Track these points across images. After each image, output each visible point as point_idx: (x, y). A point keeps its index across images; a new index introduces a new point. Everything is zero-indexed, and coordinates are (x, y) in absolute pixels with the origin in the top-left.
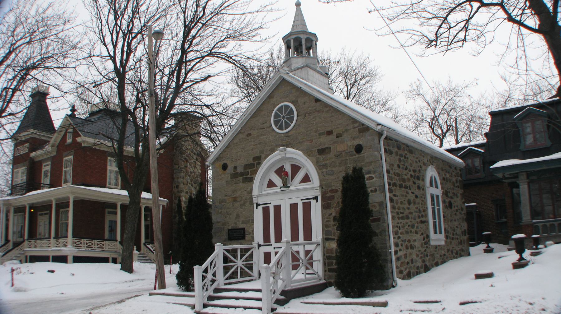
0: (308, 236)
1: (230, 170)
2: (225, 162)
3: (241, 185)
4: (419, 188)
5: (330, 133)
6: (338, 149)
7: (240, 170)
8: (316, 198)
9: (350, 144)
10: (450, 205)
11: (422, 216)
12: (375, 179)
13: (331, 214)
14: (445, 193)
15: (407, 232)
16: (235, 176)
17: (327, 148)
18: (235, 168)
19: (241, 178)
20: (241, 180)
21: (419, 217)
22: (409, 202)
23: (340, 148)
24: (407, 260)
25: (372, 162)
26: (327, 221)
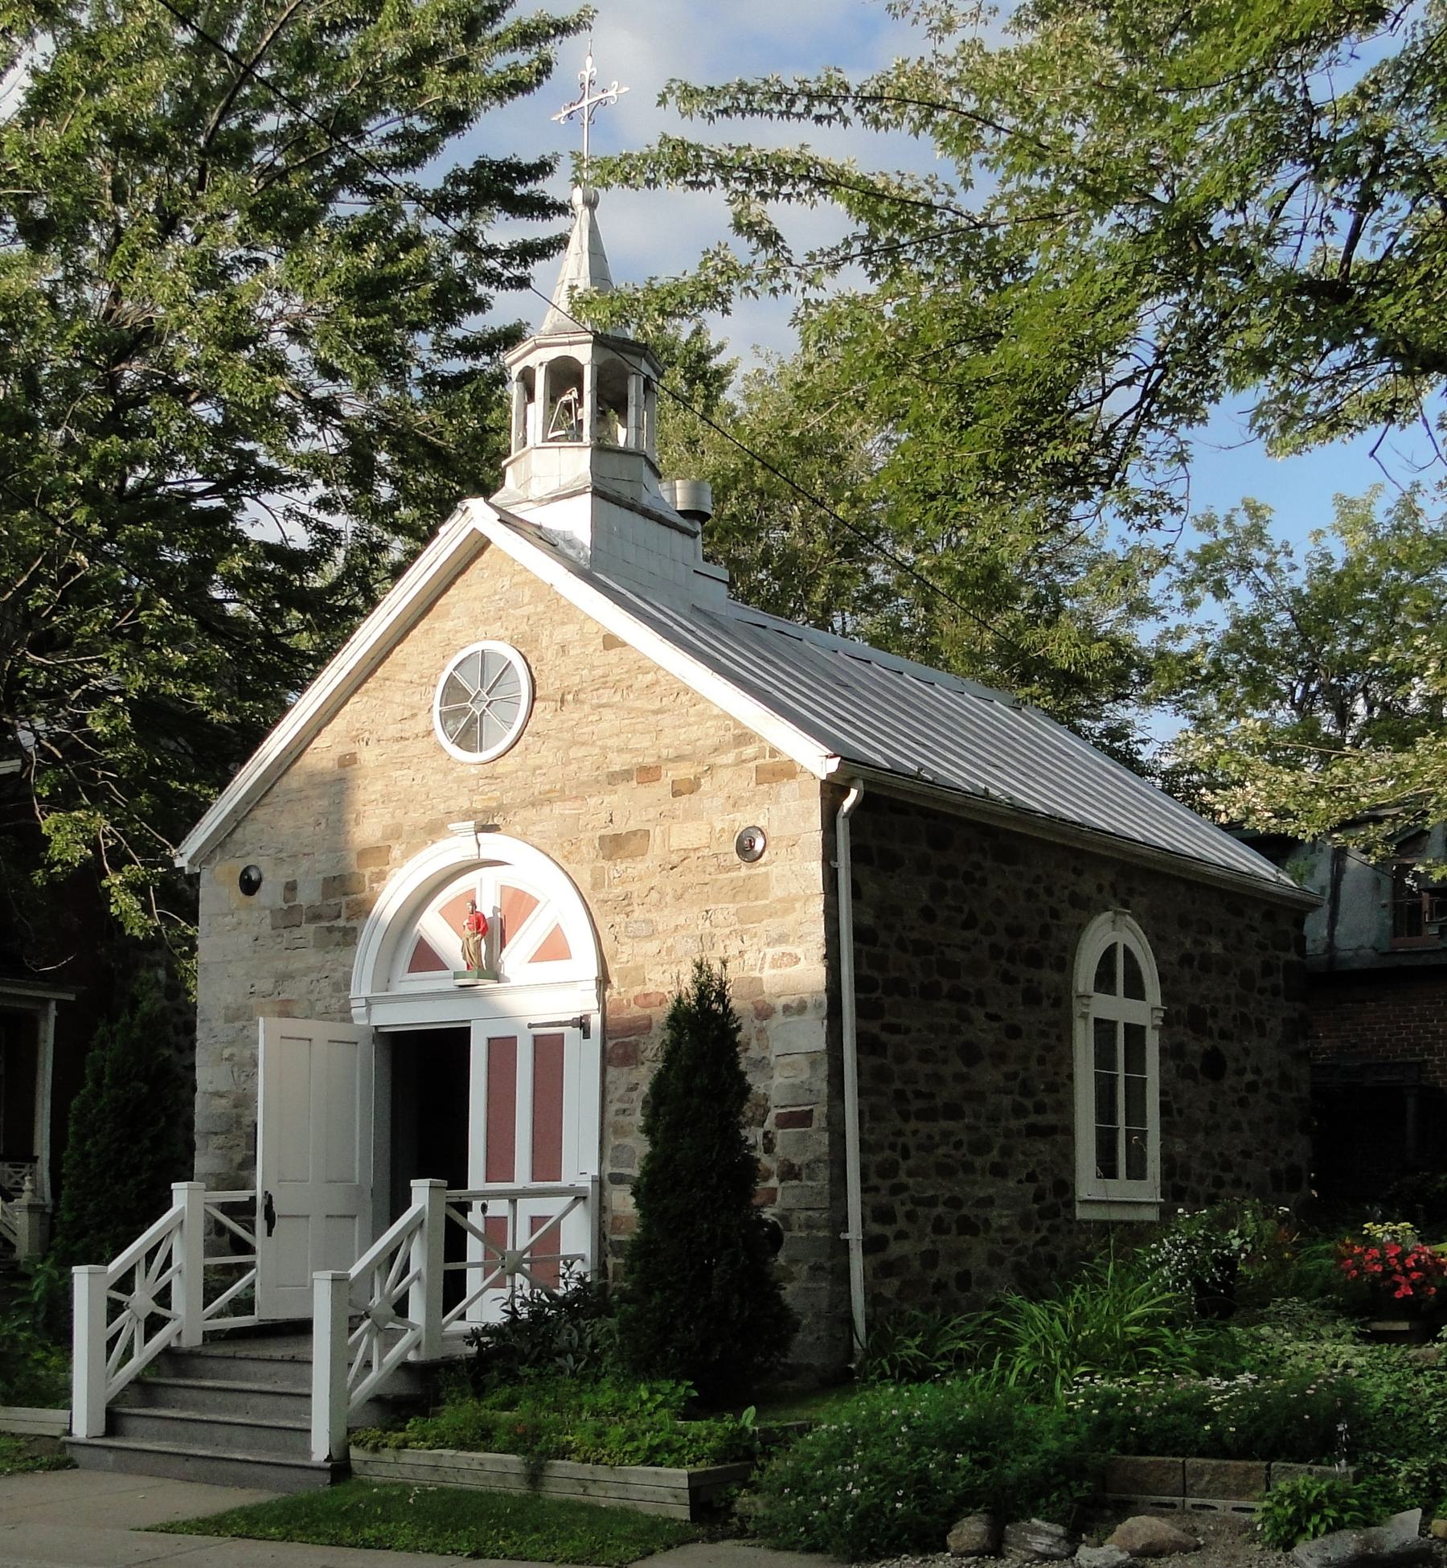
0: (547, 1160)
1: (270, 894)
2: (250, 861)
3: (312, 958)
4: (1032, 997)
5: (647, 774)
6: (675, 843)
7: (308, 896)
8: (582, 1024)
9: (718, 826)
10: (1214, 1065)
11: (1040, 1108)
12: (802, 964)
13: (634, 1088)
14: (1180, 1016)
15: (945, 1170)
16: (288, 917)
17: (635, 833)
18: (291, 887)
19: (312, 927)
20: (311, 937)
21: (1019, 1111)
22: (970, 1053)
23: (687, 835)
24: (933, 1276)
25: (796, 899)
26: (617, 1113)
